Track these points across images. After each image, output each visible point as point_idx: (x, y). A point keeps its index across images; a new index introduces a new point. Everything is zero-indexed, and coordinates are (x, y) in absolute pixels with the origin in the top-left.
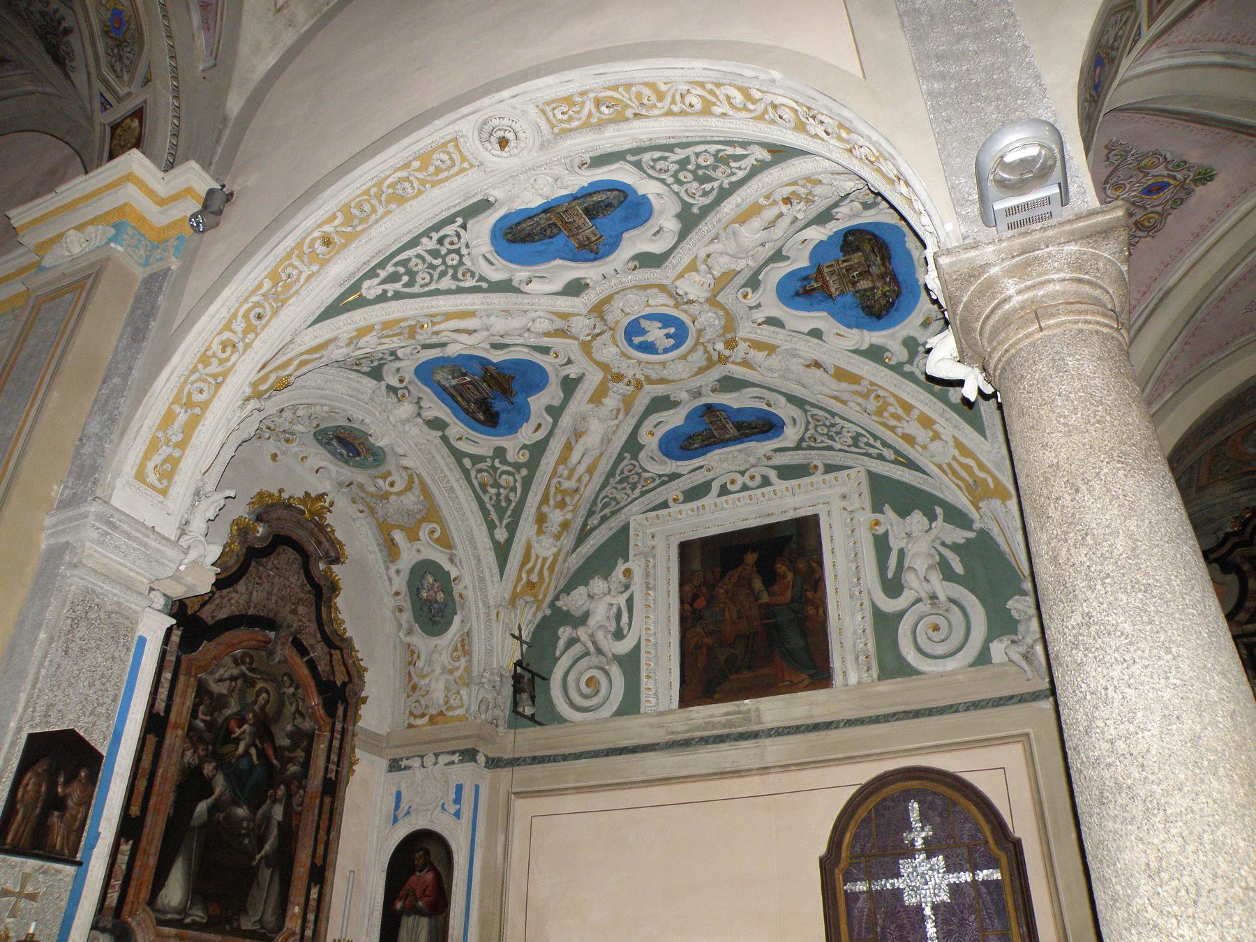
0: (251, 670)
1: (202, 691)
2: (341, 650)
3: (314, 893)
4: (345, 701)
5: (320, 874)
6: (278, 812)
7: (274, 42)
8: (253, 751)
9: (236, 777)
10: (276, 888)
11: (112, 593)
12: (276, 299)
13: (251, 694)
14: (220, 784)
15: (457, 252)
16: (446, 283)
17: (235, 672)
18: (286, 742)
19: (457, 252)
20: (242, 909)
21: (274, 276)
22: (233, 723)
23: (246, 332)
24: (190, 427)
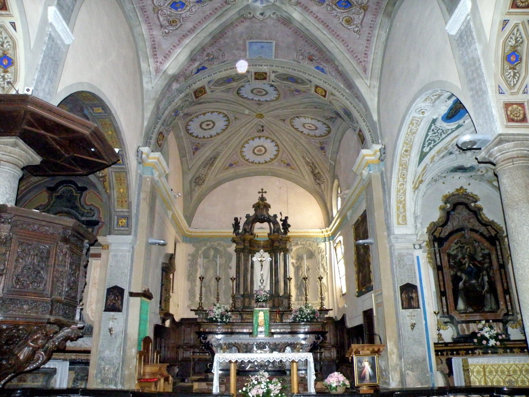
0: (462, 244)
1: (449, 255)
2: (490, 225)
3: (508, 297)
4: (498, 240)
5: (507, 291)
6: (486, 278)
7: (374, 95)
8: (471, 265)
9: (469, 273)
10: (493, 298)
11: (404, 252)
12: (405, 168)
13: (464, 251)
14: (464, 277)
15: (439, 129)
16: (444, 136)
17: (457, 246)
18: (481, 259)
19: (439, 129)
20: (484, 306)
21: (401, 165)
22: (462, 260)
23: (403, 180)
24: (404, 207)
